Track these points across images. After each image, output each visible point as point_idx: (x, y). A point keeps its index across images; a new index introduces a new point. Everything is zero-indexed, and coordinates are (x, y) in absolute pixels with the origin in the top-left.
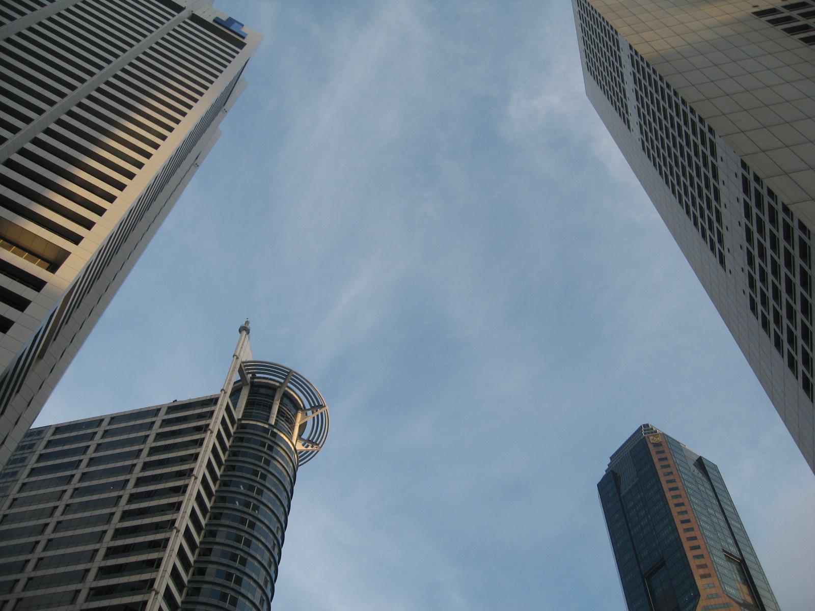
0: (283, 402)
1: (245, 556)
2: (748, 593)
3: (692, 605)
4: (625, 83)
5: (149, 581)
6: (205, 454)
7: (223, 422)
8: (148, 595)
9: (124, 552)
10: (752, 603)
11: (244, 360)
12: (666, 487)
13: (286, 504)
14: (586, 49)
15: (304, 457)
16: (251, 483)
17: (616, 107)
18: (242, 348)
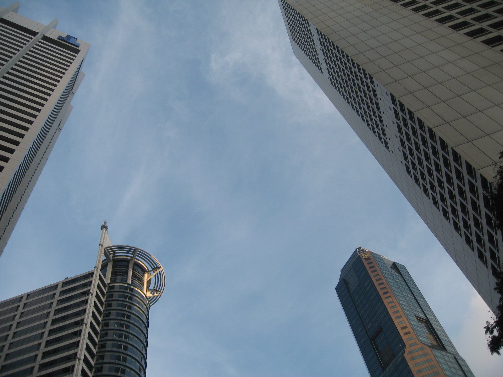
0: (135, 268)
1: (124, 368)
2: (434, 339)
3: (402, 352)
4: (313, 36)
5: (83, 310)
6: (90, 309)
7: (99, 287)
8: (75, 361)
9: (66, 301)
10: (437, 345)
11: (106, 246)
12: (376, 283)
13: (145, 331)
14: (292, 34)
15: (153, 300)
16: (123, 312)
17: (315, 63)
18: (104, 239)
